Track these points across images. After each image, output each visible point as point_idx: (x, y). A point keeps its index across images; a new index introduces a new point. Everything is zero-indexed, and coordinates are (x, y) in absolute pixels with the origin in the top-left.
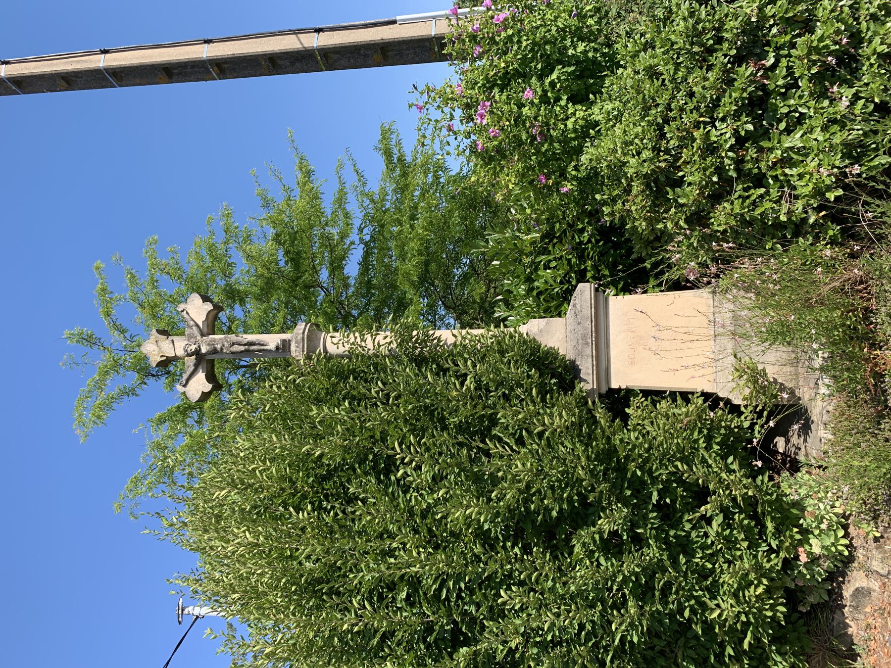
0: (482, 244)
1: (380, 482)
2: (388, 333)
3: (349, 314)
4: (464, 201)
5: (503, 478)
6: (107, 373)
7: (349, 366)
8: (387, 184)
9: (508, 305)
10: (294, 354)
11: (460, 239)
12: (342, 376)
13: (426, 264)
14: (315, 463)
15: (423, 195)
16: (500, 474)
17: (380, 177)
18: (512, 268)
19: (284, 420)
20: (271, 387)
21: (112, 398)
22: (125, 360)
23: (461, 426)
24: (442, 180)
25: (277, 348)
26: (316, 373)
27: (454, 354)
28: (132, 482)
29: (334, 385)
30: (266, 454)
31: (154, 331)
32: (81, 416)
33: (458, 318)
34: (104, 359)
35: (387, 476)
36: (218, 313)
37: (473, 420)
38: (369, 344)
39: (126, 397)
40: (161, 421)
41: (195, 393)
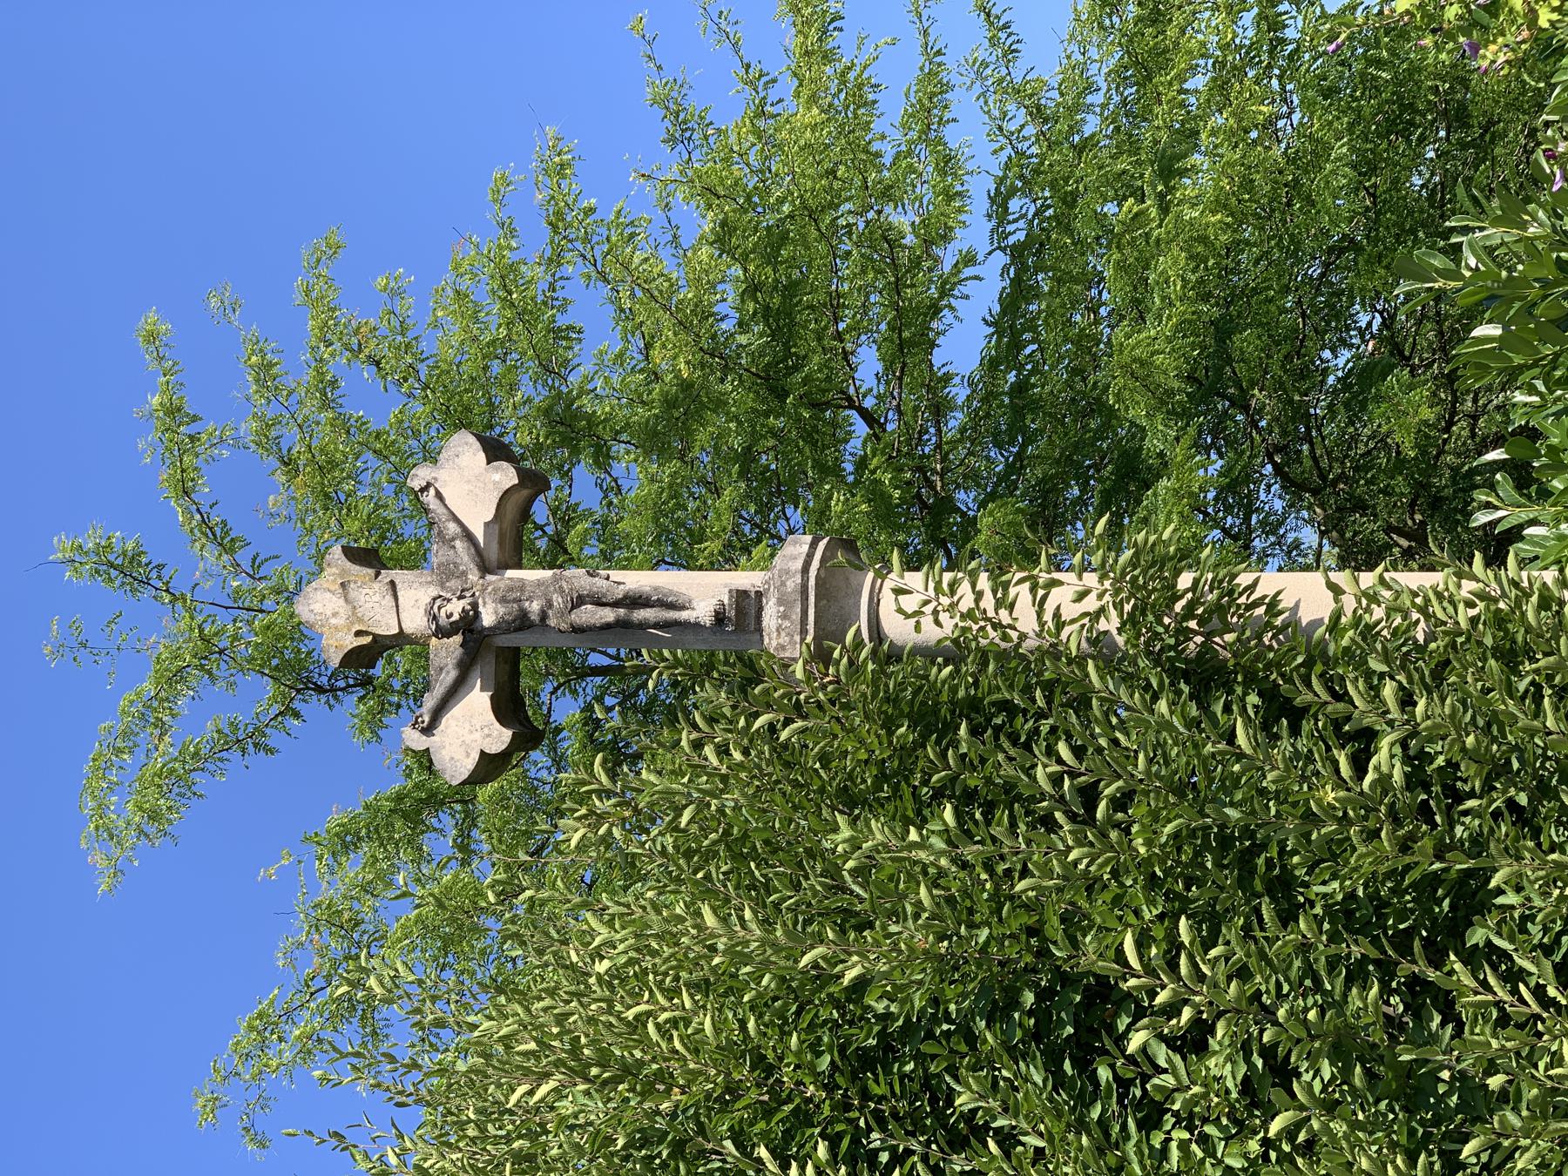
0: (1438, 262)
1: (1060, 1081)
2: (1091, 579)
3: (946, 505)
4: (1368, 106)
5: (1504, 1097)
6: (179, 675)
7: (954, 690)
8: (1094, 53)
9: (1523, 477)
10: (771, 641)
11: (1349, 244)
12: (933, 720)
13: (1223, 330)
14: (838, 1006)
15: (1220, 87)
16: (1495, 1082)
17: (1066, 26)
18: (1548, 350)
19: (739, 858)
20: (697, 745)
21: (196, 755)
22: (235, 638)
23: (1349, 914)
24: (1290, 33)
25: (720, 617)
26: (847, 707)
27: (1317, 654)
28: (251, 1028)
29: (907, 753)
30: (679, 967)
31: (337, 551)
32: (102, 809)
33: (1331, 527)
34: (168, 634)
35: (1085, 1066)
36: (530, 501)
37: (1397, 891)
38: (1025, 618)
39: (235, 754)
40: (346, 841)
41: (459, 755)
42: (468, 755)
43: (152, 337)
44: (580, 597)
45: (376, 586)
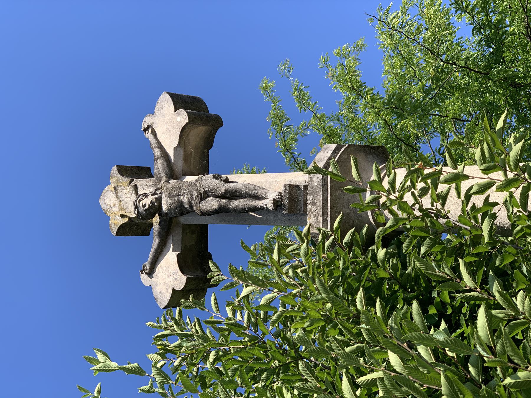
25: (277, 204)
42: (167, 290)
43: (266, 89)
44: (205, 192)
45: (128, 188)
